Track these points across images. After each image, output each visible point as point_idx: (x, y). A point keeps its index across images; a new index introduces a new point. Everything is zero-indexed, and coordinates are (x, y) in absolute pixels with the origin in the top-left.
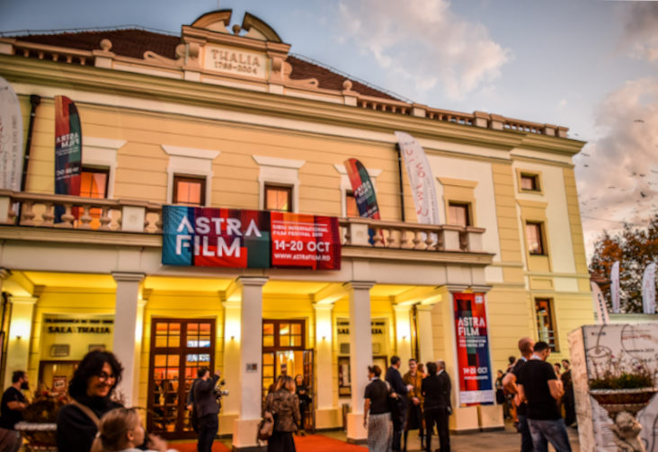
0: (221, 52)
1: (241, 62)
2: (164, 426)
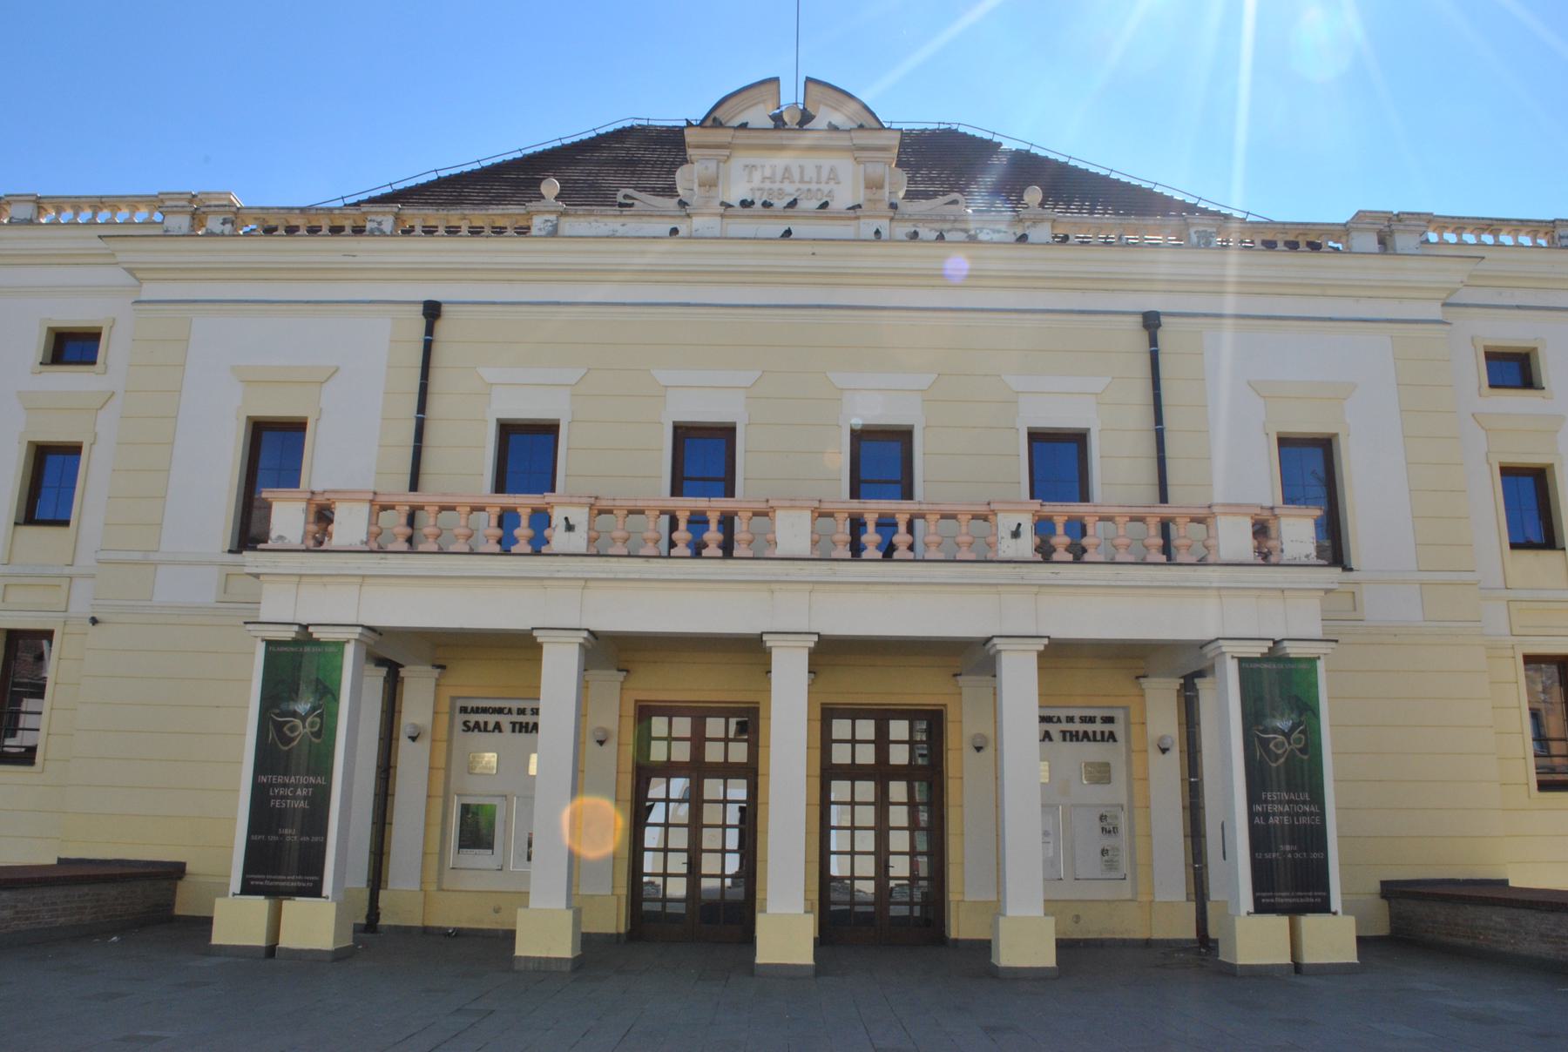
0: (763, 167)
1: (802, 181)
2: (728, 876)
